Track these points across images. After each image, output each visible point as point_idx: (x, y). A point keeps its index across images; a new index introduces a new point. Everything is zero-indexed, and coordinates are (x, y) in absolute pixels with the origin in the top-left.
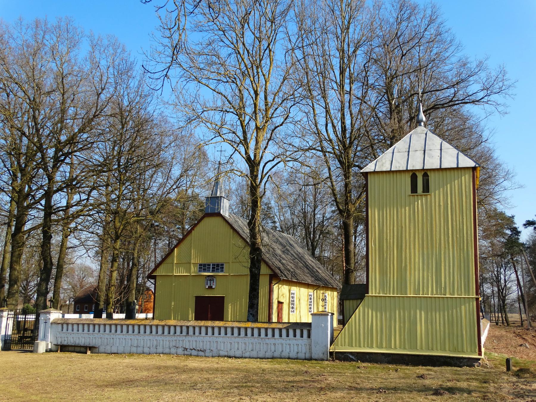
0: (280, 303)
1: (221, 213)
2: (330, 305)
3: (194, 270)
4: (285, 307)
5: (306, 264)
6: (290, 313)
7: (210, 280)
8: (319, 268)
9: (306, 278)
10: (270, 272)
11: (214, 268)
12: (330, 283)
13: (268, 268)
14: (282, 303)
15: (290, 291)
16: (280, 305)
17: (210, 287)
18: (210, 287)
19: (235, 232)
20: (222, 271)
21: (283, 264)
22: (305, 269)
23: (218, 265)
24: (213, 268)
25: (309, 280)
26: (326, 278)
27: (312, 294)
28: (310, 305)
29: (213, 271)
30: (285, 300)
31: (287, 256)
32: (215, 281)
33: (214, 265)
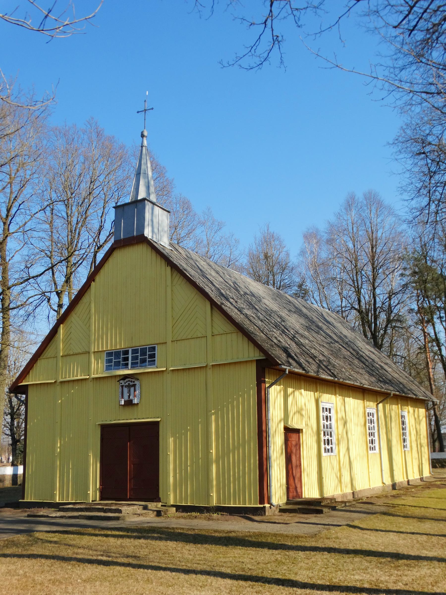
0: (291, 433)
1: (148, 233)
2: (413, 433)
3: (97, 368)
4: (308, 442)
5: (358, 353)
6: (324, 454)
7: (129, 386)
8: (386, 364)
9: (358, 377)
10: (256, 355)
11: (136, 358)
12: (410, 390)
13: (252, 345)
14: (298, 431)
15: (317, 401)
16: (294, 436)
17: (129, 403)
18: (129, 403)
19: (175, 273)
20: (152, 362)
21: (299, 344)
22: (356, 362)
23: (143, 352)
24: (133, 358)
25: (365, 381)
26: (401, 380)
27: (374, 411)
28: (371, 434)
29: (134, 365)
30: (307, 423)
31: (315, 335)
32: (137, 387)
33: (135, 351)
